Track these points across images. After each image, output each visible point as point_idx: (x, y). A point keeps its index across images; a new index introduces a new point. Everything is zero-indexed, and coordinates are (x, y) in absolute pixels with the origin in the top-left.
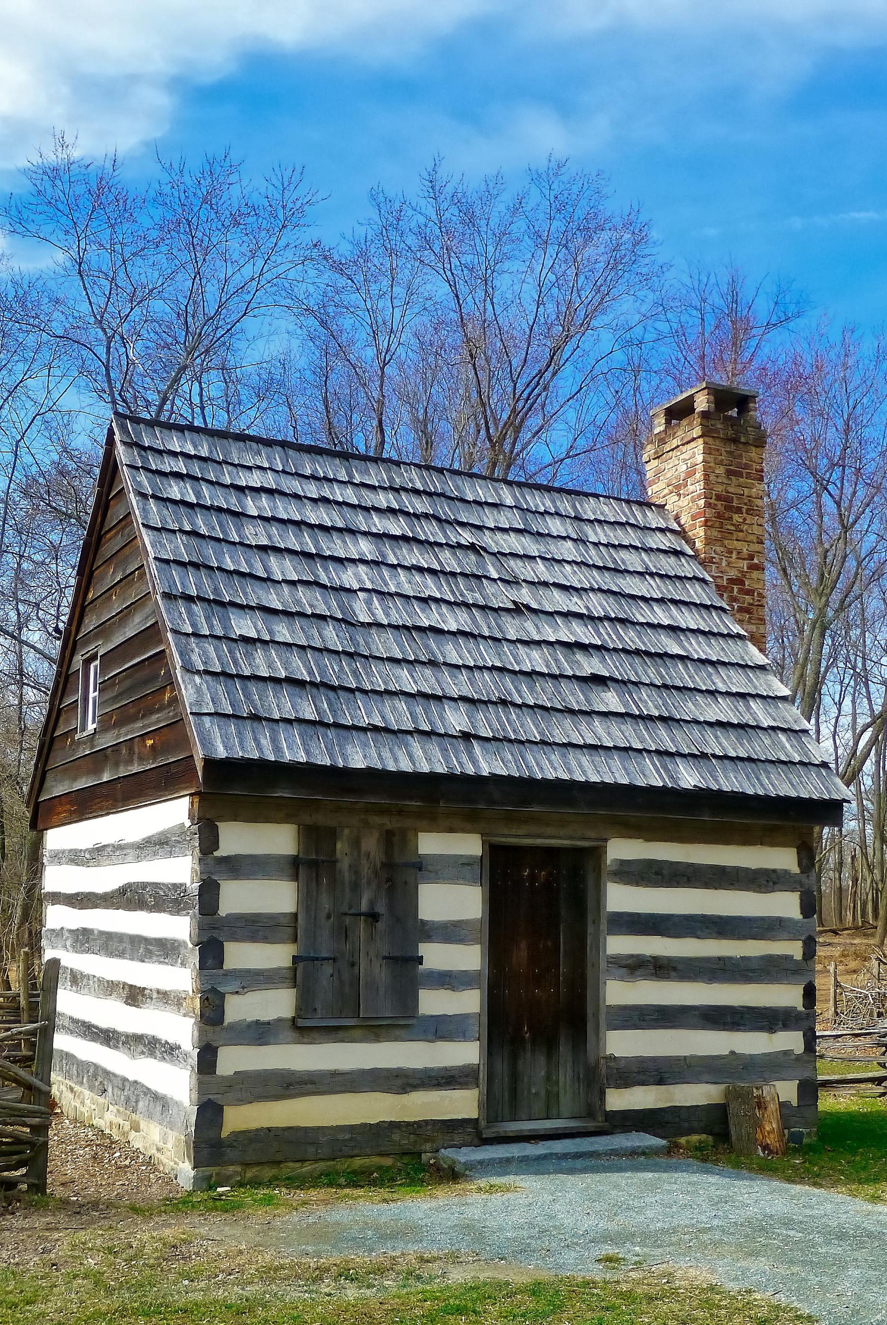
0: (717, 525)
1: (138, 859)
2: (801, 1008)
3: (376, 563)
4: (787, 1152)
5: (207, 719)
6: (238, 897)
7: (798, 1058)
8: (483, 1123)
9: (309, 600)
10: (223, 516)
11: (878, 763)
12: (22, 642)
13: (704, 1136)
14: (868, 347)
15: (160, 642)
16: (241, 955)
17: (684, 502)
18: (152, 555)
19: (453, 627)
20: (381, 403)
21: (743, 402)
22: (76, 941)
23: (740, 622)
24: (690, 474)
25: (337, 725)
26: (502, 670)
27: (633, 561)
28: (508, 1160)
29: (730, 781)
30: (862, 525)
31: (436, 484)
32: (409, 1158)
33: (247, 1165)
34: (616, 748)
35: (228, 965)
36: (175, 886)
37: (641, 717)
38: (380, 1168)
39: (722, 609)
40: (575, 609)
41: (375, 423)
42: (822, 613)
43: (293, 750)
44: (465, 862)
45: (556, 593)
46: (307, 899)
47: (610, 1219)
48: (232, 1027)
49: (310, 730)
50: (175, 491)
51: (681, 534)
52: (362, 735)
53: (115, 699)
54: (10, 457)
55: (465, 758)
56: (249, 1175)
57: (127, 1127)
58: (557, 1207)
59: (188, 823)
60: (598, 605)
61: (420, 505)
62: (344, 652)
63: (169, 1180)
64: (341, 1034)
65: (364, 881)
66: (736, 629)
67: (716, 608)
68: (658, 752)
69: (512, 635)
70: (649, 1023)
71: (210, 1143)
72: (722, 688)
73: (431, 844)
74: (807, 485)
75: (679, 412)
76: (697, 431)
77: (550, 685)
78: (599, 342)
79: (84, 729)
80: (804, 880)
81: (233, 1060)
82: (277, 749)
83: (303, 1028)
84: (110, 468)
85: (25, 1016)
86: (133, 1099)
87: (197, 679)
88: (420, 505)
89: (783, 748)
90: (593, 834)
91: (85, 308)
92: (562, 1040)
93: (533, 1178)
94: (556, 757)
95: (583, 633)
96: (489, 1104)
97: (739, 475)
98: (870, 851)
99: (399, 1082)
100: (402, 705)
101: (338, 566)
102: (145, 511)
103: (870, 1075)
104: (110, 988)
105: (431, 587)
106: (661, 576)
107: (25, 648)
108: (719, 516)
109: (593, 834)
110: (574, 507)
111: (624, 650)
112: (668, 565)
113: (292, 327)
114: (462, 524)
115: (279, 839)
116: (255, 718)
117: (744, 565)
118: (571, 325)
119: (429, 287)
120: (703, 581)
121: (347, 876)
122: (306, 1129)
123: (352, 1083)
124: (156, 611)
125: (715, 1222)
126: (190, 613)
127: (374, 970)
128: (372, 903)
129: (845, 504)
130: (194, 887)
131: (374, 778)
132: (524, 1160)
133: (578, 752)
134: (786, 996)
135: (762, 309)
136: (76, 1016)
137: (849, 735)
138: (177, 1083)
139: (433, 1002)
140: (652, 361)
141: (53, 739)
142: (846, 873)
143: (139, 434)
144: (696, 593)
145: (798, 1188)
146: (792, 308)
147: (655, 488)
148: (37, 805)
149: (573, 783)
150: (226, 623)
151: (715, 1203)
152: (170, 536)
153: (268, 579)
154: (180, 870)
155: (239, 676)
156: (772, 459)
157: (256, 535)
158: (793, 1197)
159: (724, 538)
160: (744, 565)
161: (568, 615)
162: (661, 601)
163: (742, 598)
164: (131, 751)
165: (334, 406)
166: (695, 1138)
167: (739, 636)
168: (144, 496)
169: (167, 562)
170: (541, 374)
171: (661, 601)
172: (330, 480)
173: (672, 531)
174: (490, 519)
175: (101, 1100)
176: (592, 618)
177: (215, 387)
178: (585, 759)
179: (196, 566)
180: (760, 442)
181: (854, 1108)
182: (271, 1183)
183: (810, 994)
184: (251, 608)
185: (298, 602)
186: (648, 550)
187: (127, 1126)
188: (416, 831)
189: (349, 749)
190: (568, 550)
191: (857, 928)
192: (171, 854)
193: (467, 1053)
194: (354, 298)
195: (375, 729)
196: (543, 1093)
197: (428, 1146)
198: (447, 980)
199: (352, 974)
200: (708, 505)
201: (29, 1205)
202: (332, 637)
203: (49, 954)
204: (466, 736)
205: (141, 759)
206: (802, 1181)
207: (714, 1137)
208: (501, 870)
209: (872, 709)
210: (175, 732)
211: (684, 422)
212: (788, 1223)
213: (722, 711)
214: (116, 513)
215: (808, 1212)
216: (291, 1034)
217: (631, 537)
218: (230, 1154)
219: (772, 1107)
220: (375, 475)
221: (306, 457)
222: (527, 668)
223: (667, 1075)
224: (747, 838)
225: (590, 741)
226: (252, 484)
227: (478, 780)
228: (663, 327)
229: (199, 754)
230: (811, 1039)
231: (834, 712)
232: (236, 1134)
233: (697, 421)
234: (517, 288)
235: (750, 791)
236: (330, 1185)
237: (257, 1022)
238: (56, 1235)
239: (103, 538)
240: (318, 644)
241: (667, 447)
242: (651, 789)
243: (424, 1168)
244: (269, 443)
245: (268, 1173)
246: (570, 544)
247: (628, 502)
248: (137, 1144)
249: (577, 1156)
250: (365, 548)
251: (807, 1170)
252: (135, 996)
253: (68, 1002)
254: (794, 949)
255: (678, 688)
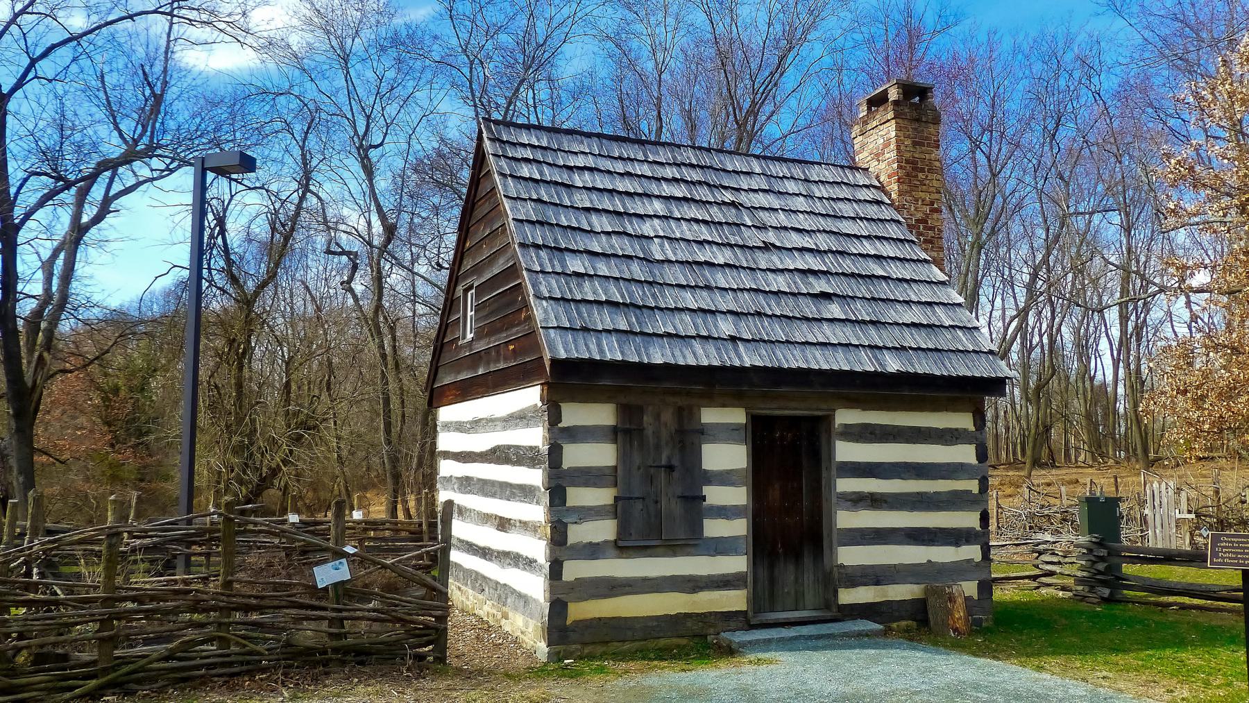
1: (504, 429)
2: (978, 528)
3: (666, 217)
4: (972, 633)
5: (552, 331)
6: (577, 455)
8: (750, 614)
9: (620, 245)
10: (559, 188)
11: (1022, 343)
12: (414, 273)
13: (910, 622)
14: (1006, 45)
15: (518, 277)
16: (579, 496)
17: (883, 165)
18: (511, 217)
19: (721, 261)
20: (659, 99)
21: (923, 92)
22: (461, 485)
23: (925, 250)
24: (887, 145)
25: (642, 334)
26: (757, 291)
27: (846, 209)
28: (769, 641)
29: (923, 366)
30: (1007, 172)
31: (706, 160)
32: (697, 639)
33: (585, 644)
34: (840, 344)
35: (569, 503)
36: (531, 448)
37: (857, 322)
38: (678, 646)
39: (913, 242)
40: (806, 245)
41: (655, 113)
42: (979, 236)
43: (612, 351)
44: (734, 428)
45: (794, 235)
46: (623, 456)
47: (847, 684)
48: (573, 547)
49: (624, 337)
50: (525, 171)
51: (881, 188)
52: (660, 340)
53: (486, 317)
54: (405, 146)
55: (733, 355)
56: (586, 651)
57: (499, 616)
58: (807, 675)
59: (540, 404)
60: (823, 242)
61: (695, 175)
62: (646, 281)
63: (531, 654)
64: (649, 551)
66: (923, 256)
67: (908, 241)
68: (869, 346)
69: (763, 265)
70: (869, 542)
71: (559, 629)
72: (914, 298)
73: (710, 416)
74: (966, 146)
75: (878, 101)
76: (890, 115)
77: (791, 301)
78: (814, 50)
79: (464, 337)
80: (979, 435)
81: (574, 570)
82: (601, 351)
83: (622, 547)
84: (480, 156)
85: (426, 537)
86: (503, 596)
87: (544, 303)
88: (695, 175)
89: (961, 341)
91: (454, 41)
92: (806, 553)
93: (788, 653)
94: (797, 352)
95: (814, 263)
96: (754, 600)
97: (922, 144)
98: (1018, 407)
99: (691, 585)
100: (687, 318)
101: (640, 220)
102: (505, 186)
103: (1027, 573)
104: (486, 518)
105: (705, 233)
106: (867, 219)
107: (417, 277)
108: (908, 175)
109: (824, 406)
110: (804, 172)
111: (843, 274)
112: (872, 211)
113: (596, 49)
114: (725, 188)
115: (602, 415)
116: (585, 329)
117: (927, 209)
118: (791, 41)
119: (691, 17)
120: (898, 222)
121: (651, 440)
123: (657, 582)
124: (514, 256)
125: (923, 687)
126: (538, 257)
127: (672, 506)
128: (669, 458)
129: (993, 157)
130: (544, 449)
131: (669, 370)
132: (781, 640)
133: (813, 348)
134: (969, 520)
135: (930, 20)
136: (462, 538)
137: (1000, 324)
138: (535, 586)
139: (714, 528)
140: (851, 62)
141: (442, 345)
142: (1001, 423)
143: (499, 133)
144: (893, 231)
145: (982, 660)
146: (951, 19)
147: (861, 156)
148: (432, 390)
149: (810, 371)
150: (563, 263)
151: (923, 672)
152: (523, 203)
153: (591, 231)
154: (535, 436)
155: (573, 300)
156: (947, 130)
157: (583, 200)
158: (979, 667)
160: (927, 209)
161: (802, 250)
162: (868, 237)
163: (926, 232)
164: (498, 353)
165: (627, 103)
166: (904, 623)
167: (925, 261)
168: (504, 175)
169: (521, 221)
170: (772, 74)
171: (868, 237)
172: (632, 160)
173: (875, 187)
174: (744, 183)
175: (481, 597)
176: (819, 252)
177: (543, 92)
178: (818, 352)
179: (541, 223)
180: (937, 121)
181: (1017, 598)
182: (602, 657)
183: (985, 518)
184: (581, 252)
185: (612, 247)
186: (858, 201)
187: (499, 615)
188: (699, 407)
189: (651, 350)
190: (801, 204)
191: (1010, 464)
192: (528, 426)
193: (738, 564)
194: (639, 27)
195: (669, 335)
196: (793, 592)
197: (712, 630)
198: (723, 512)
199: (657, 509)
200: (900, 167)
201: (435, 672)
202: (637, 271)
203: (443, 496)
204: (733, 339)
205: (506, 359)
206: (984, 656)
207: (917, 623)
208: (761, 436)
209: (1017, 305)
210: (530, 340)
211: (881, 109)
212: (977, 687)
213: (911, 315)
214: (484, 188)
215: (991, 679)
216: (613, 552)
217: (844, 192)
218: (573, 636)
219: (960, 600)
220: (663, 155)
221: (614, 144)
222: (775, 289)
225: (821, 340)
226: (578, 164)
227: (742, 369)
228: (858, 37)
229: (547, 356)
230: (986, 549)
231: (988, 308)
232: (576, 622)
233: (890, 107)
234: (753, 14)
235: (938, 373)
236: (643, 658)
237: (590, 543)
238: (455, 694)
239: (477, 207)
240: (627, 276)
241: (869, 127)
242: (866, 374)
243: (709, 646)
244: (589, 135)
245: (599, 649)
246: (802, 198)
247: (842, 167)
248: (507, 628)
249: (819, 637)
250: (658, 207)
251: (987, 647)
252: (503, 524)
253: (460, 529)
254: (973, 486)
255: (883, 300)
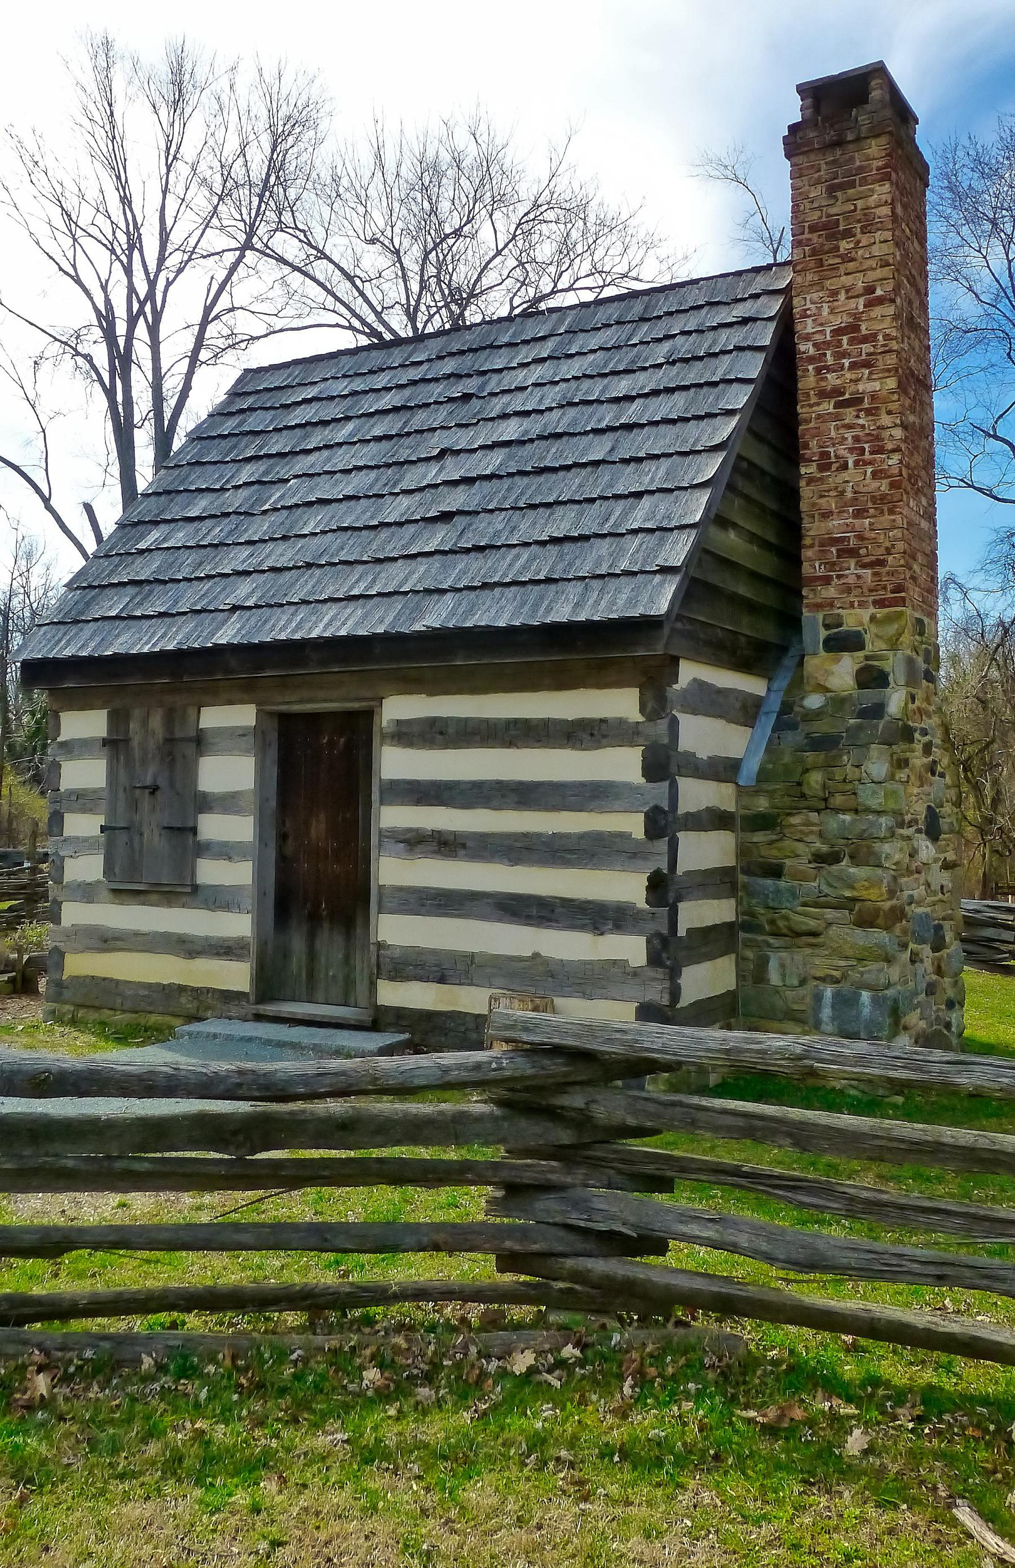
0: (812, 264)
7: (635, 973)
35: (67, 832)
44: (241, 733)
48: (68, 886)
64: (142, 898)
65: (150, 756)
73: (213, 717)
90: (368, 694)
122: (117, 982)
159: (823, 279)
193: (239, 925)
196: (340, 977)
198: (226, 851)
223: (451, 973)
224: (562, 680)
